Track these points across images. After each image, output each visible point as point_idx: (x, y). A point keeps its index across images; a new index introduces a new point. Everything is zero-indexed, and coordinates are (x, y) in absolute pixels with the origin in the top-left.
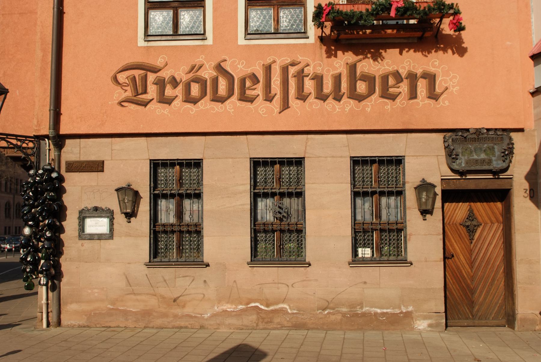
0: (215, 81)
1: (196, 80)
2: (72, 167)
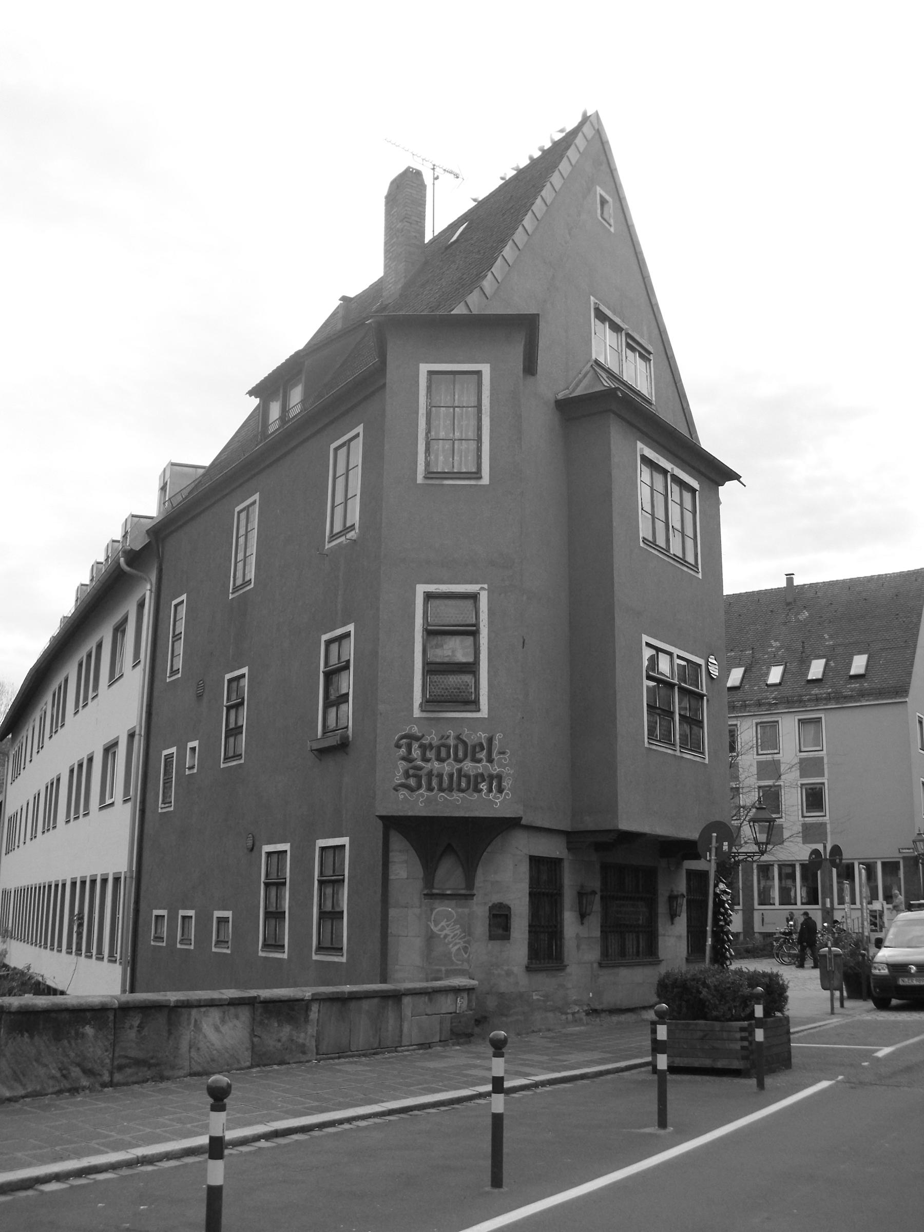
0: (456, 747)
1: (444, 745)
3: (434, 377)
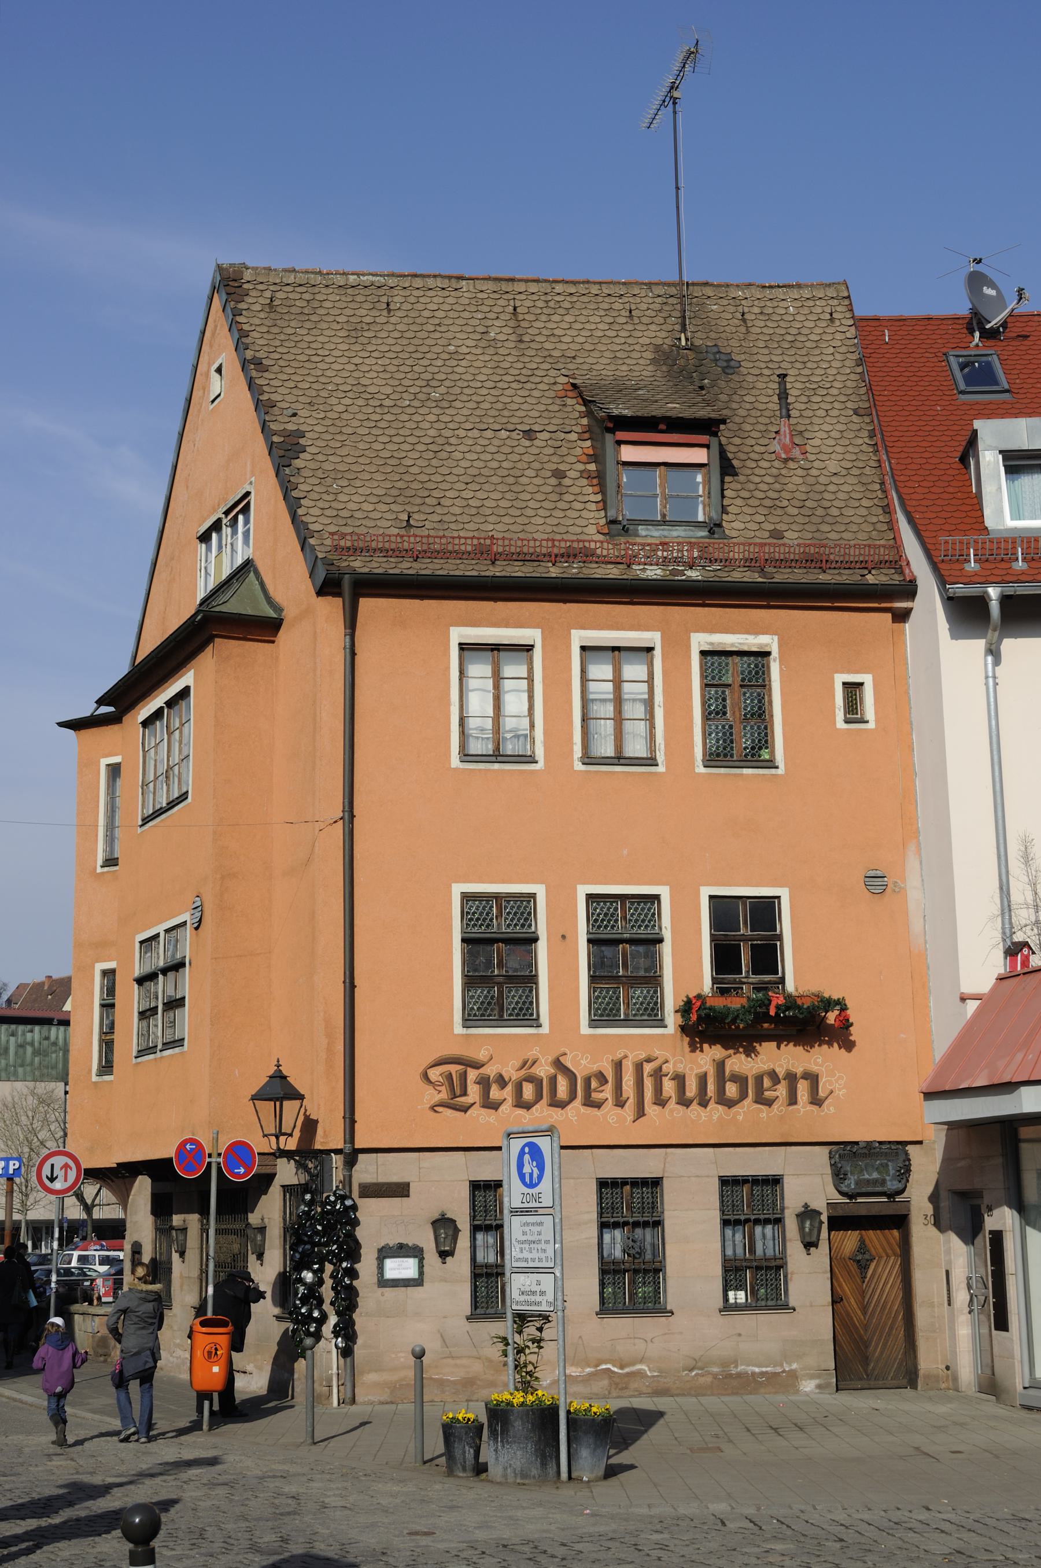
0: (553, 1080)
1: (530, 1079)
3: (588, 653)
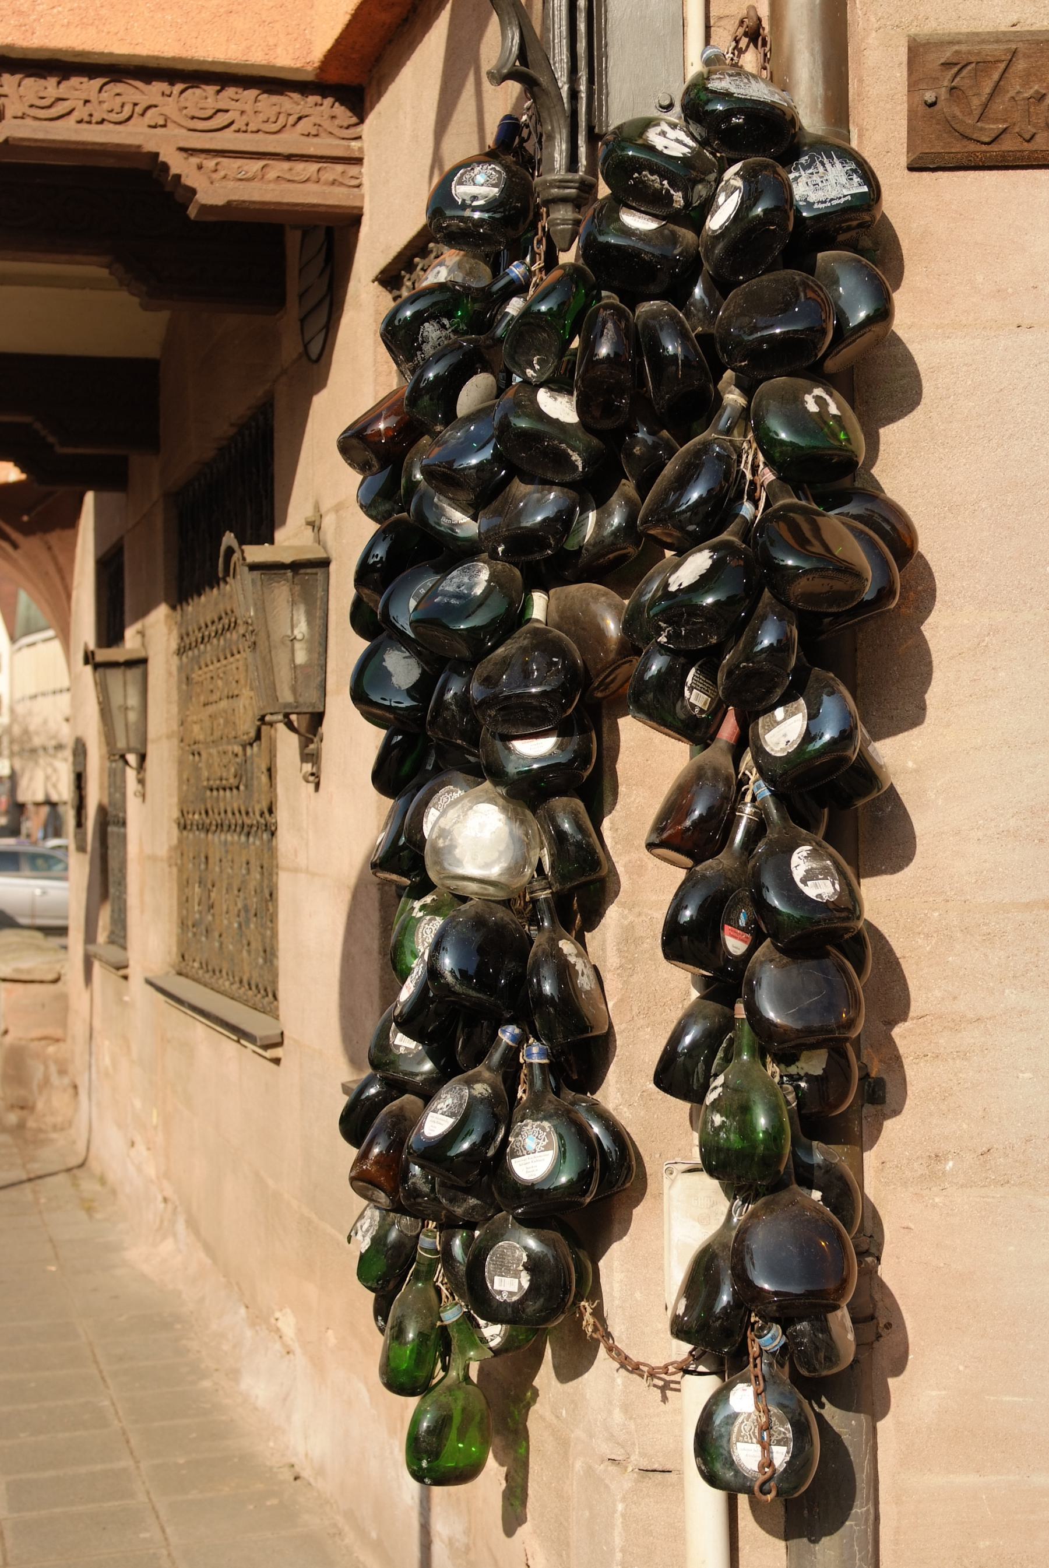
2: (999, 106)
